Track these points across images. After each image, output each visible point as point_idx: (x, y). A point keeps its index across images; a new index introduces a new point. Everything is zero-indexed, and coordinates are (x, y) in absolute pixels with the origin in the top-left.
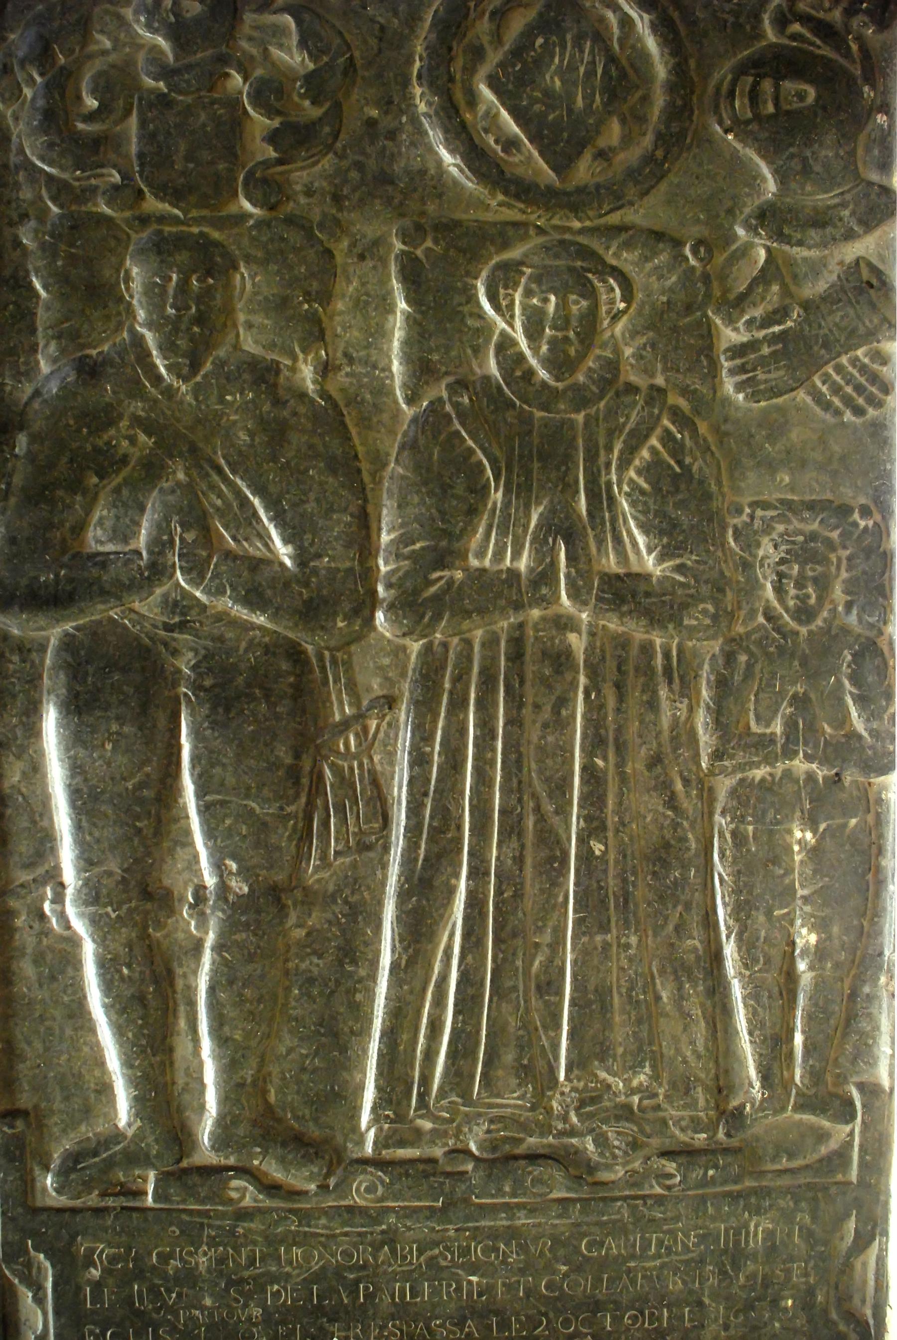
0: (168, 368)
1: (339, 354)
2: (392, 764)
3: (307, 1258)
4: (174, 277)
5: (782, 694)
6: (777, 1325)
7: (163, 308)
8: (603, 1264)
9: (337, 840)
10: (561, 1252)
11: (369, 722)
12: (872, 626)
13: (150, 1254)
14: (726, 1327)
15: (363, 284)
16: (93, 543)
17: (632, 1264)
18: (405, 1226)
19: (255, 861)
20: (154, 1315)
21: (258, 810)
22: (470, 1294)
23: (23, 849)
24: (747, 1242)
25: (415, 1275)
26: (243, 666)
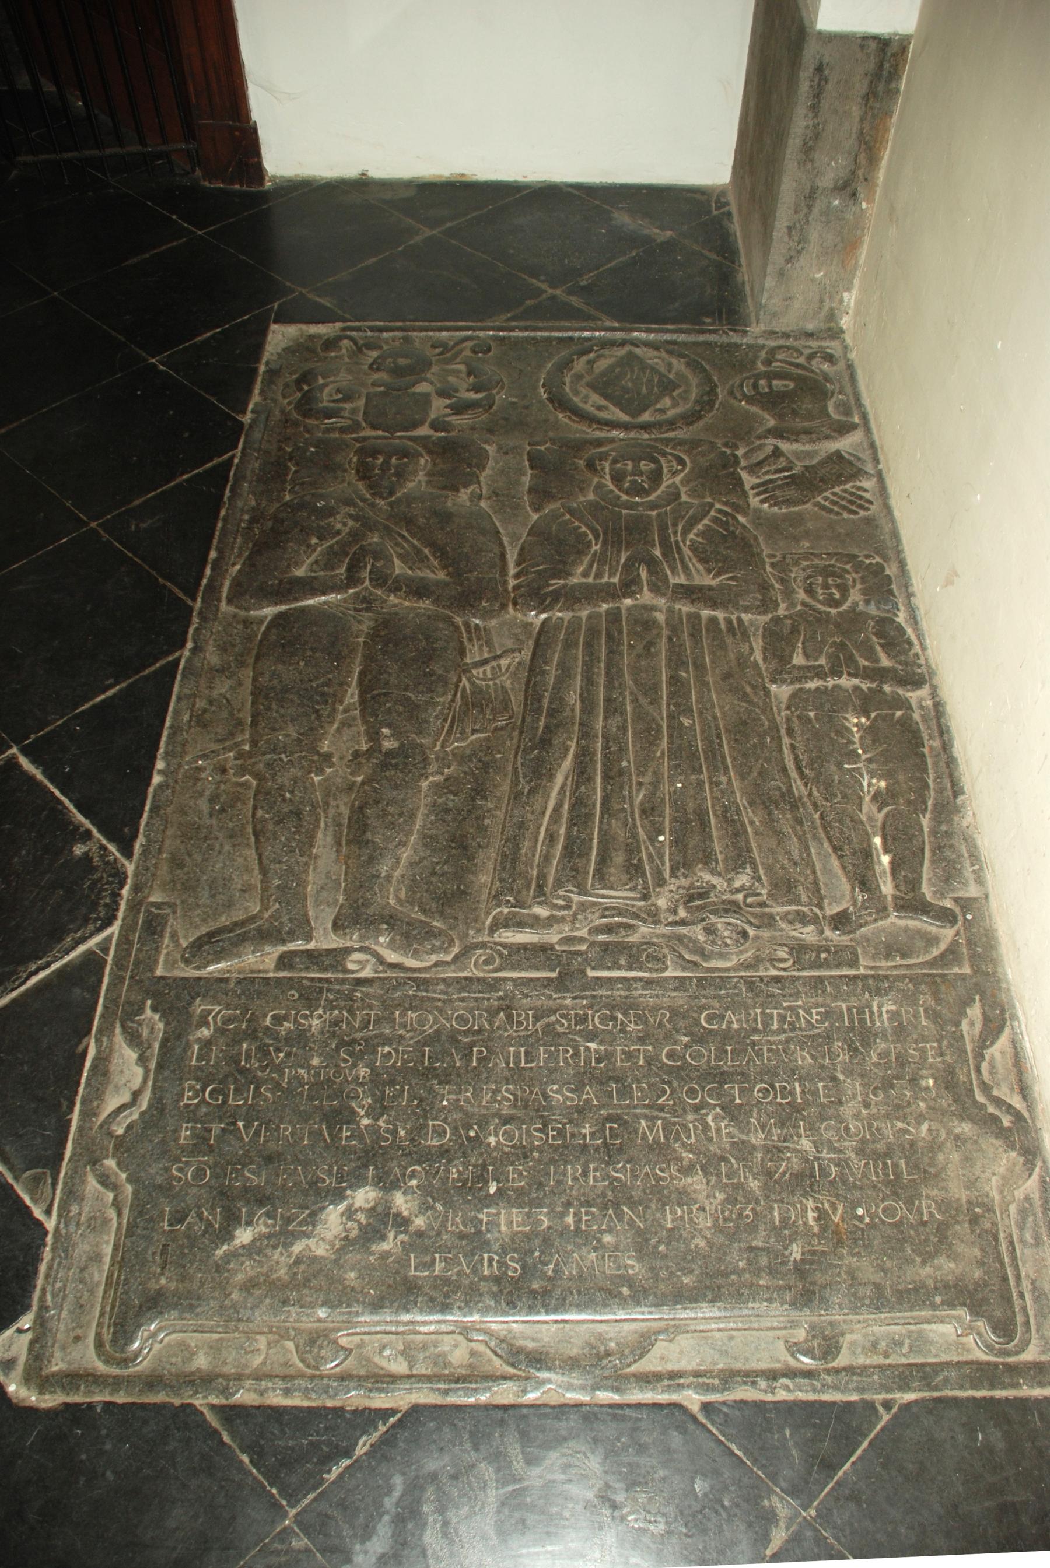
3: (422, 1022)
5: (824, 642)
6: (921, 1104)
8: (726, 1036)
10: (682, 1024)
12: (889, 611)
13: (265, 1016)
14: (867, 1105)
17: (756, 1038)
18: (522, 993)
20: (259, 1074)
22: (588, 1061)
24: (872, 1021)
25: (532, 1040)
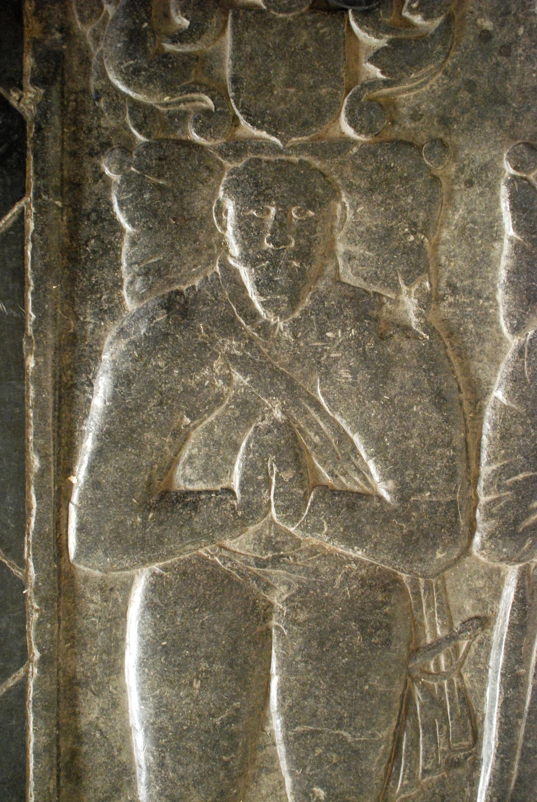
0: (264, 305)
1: (443, 284)
2: (483, 681)
4: (273, 210)
7: (260, 241)
9: (426, 759)
11: (460, 642)
15: (470, 212)
16: (181, 482)
19: (345, 787)
21: (350, 739)
23: (98, 784)
26: (338, 599)
